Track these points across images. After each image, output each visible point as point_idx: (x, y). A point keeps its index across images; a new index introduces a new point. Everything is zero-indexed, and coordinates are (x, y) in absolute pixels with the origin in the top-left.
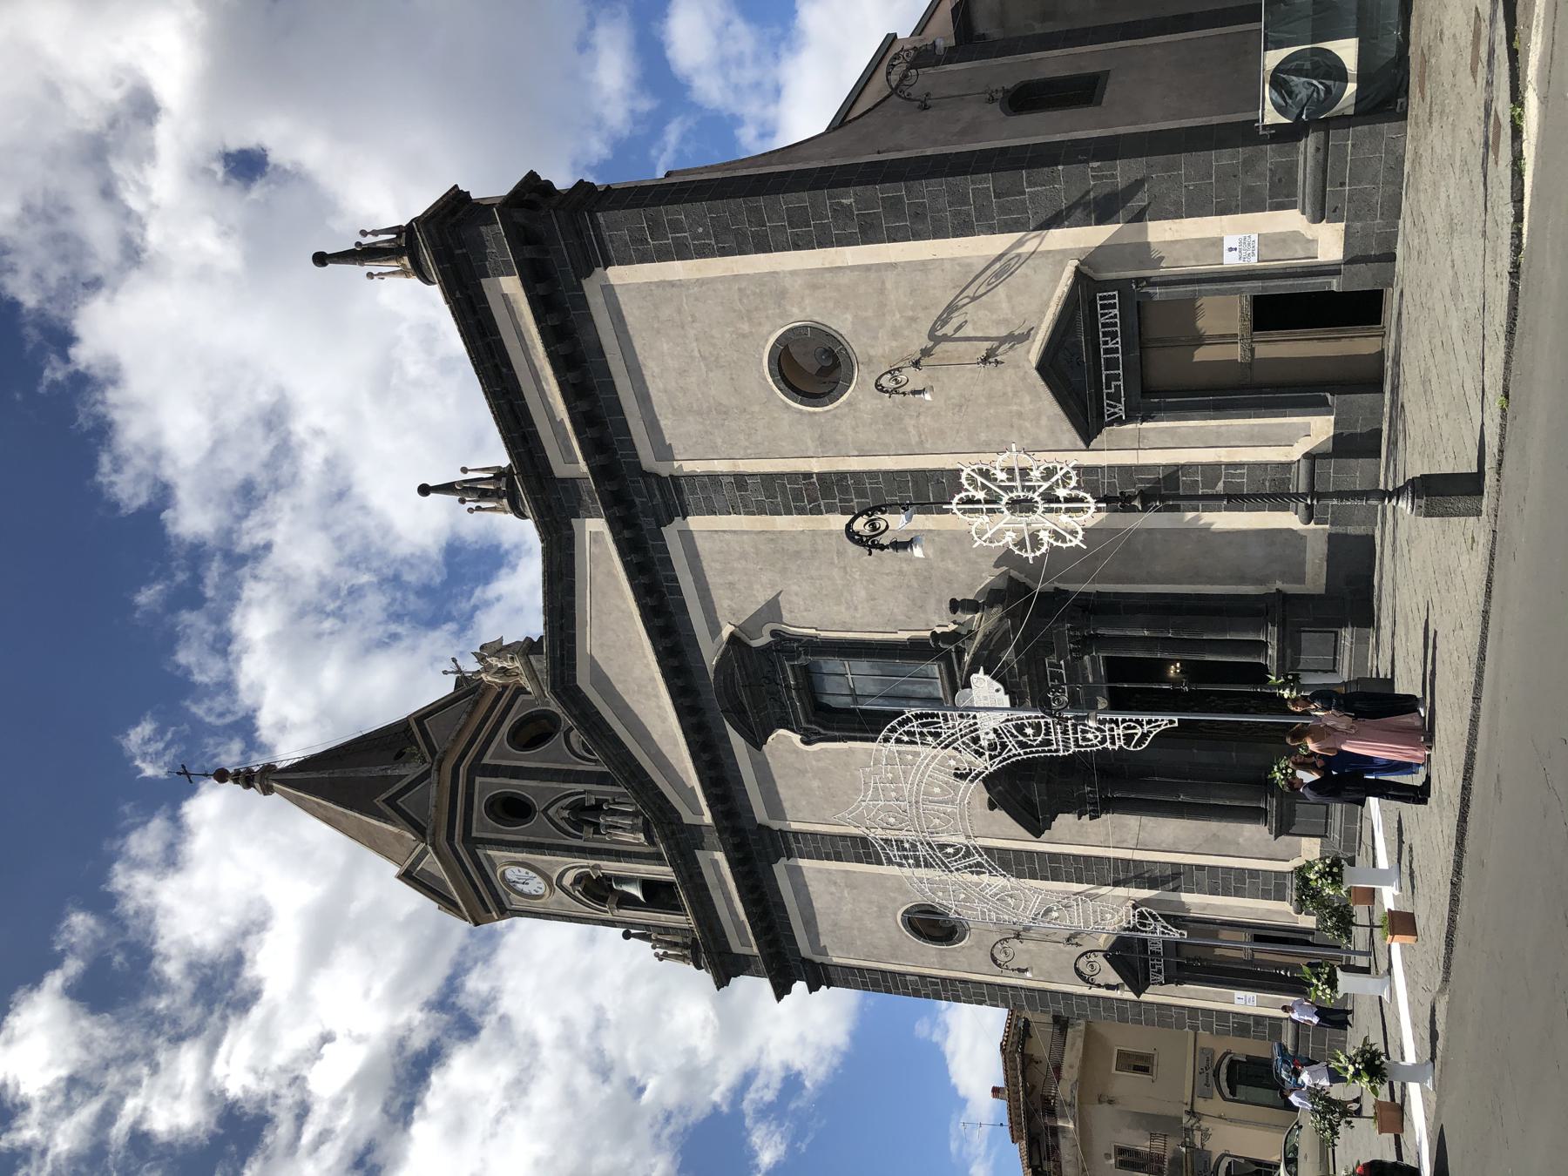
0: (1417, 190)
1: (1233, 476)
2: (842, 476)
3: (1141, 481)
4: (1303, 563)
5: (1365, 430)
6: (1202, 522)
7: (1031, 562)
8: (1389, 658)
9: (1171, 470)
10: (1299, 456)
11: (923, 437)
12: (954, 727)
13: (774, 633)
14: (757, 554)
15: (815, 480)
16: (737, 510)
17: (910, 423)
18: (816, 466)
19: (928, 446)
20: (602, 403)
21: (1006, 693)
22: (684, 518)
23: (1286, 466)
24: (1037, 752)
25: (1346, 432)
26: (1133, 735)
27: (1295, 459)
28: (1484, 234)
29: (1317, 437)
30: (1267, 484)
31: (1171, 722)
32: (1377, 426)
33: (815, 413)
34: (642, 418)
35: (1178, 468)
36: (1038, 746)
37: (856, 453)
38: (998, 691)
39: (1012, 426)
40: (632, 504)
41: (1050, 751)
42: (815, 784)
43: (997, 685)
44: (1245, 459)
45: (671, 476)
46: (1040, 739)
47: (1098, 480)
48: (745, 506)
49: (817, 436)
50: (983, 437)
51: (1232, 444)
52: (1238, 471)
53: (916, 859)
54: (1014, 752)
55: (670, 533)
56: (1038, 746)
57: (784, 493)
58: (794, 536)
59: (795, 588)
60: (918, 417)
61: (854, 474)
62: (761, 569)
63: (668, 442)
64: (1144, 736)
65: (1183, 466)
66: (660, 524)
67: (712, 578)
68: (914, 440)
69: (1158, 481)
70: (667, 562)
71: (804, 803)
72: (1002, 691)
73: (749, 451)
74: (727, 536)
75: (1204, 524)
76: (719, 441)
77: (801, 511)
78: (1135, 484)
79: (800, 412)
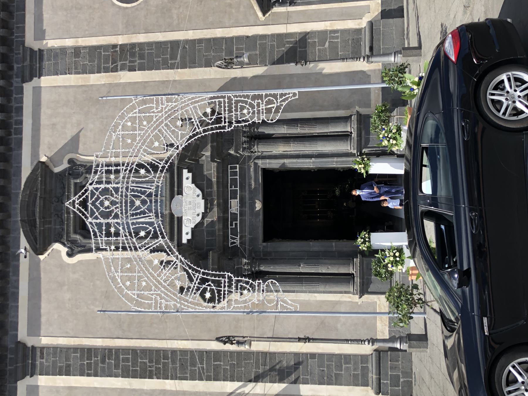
0: (416, 351)
1: (333, 38)
2: (133, 46)
3: (288, 42)
4: (370, 100)
5: (396, 7)
6: (318, 68)
7: (233, 186)
8: (415, 32)
9: (302, 35)
10: (372, 352)
11: (180, 20)
12: (162, 111)
13: (71, 161)
14: (74, 102)
15: (118, 49)
16: (70, 71)
17: (175, 12)
18: (121, 40)
19: (182, 26)
20: (15, 4)
21: (203, 199)
22: (39, 78)
23: (358, 31)
24: (212, 129)
25: (388, 8)
26: (271, 109)
27: (363, 27)
28: (435, 12)
29: (373, 13)
30: (350, 42)
31: (294, 94)
32: (401, 5)
33: (127, 8)
34: (34, 14)
35: (307, 34)
36: (213, 123)
37: (144, 32)
38: (198, 196)
39: (226, 12)
40: (11, 68)
41: (220, 128)
42: (68, 296)
43: (199, 192)
44: (339, 28)
45: (39, 49)
46: (214, 117)
47: (266, 43)
48: (76, 68)
49: (125, 21)
50: (211, 19)
51: (333, 19)
52: (336, 35)
53: (116, 243)
54: (198, 130)
55: (28, 88)
56: (213, 123)
57: (100, 58)
58: (98, 87)
59: (91, 126)
60: (179, 8)
61: (141, 45)
62: (74, 113)
63: (44, 28)
64: (278, 108)
65: (308, 33)
66: (24, 81)
67: (44, 120)
68: (175, 22)
69: (296, 42)
70: (20, 110)
71: (56, 316)
72: (201, 196)
73: (87, 32)
74: (60, 90)
75: (319, 69)
76: (72, 26)
77: (106, 70)
78: (285, 45)
79: (119, 7)
